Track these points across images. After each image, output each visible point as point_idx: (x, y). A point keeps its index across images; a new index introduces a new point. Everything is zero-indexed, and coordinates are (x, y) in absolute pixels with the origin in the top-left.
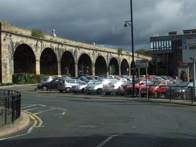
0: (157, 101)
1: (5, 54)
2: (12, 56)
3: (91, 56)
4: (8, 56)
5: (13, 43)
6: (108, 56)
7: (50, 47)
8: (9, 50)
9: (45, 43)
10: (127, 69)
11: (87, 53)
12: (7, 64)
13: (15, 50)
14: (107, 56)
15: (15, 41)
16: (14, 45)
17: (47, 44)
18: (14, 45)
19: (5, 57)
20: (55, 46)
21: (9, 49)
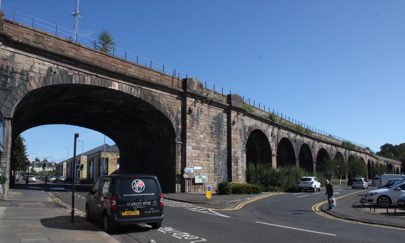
8: (241, 138)
20: (292, 135)
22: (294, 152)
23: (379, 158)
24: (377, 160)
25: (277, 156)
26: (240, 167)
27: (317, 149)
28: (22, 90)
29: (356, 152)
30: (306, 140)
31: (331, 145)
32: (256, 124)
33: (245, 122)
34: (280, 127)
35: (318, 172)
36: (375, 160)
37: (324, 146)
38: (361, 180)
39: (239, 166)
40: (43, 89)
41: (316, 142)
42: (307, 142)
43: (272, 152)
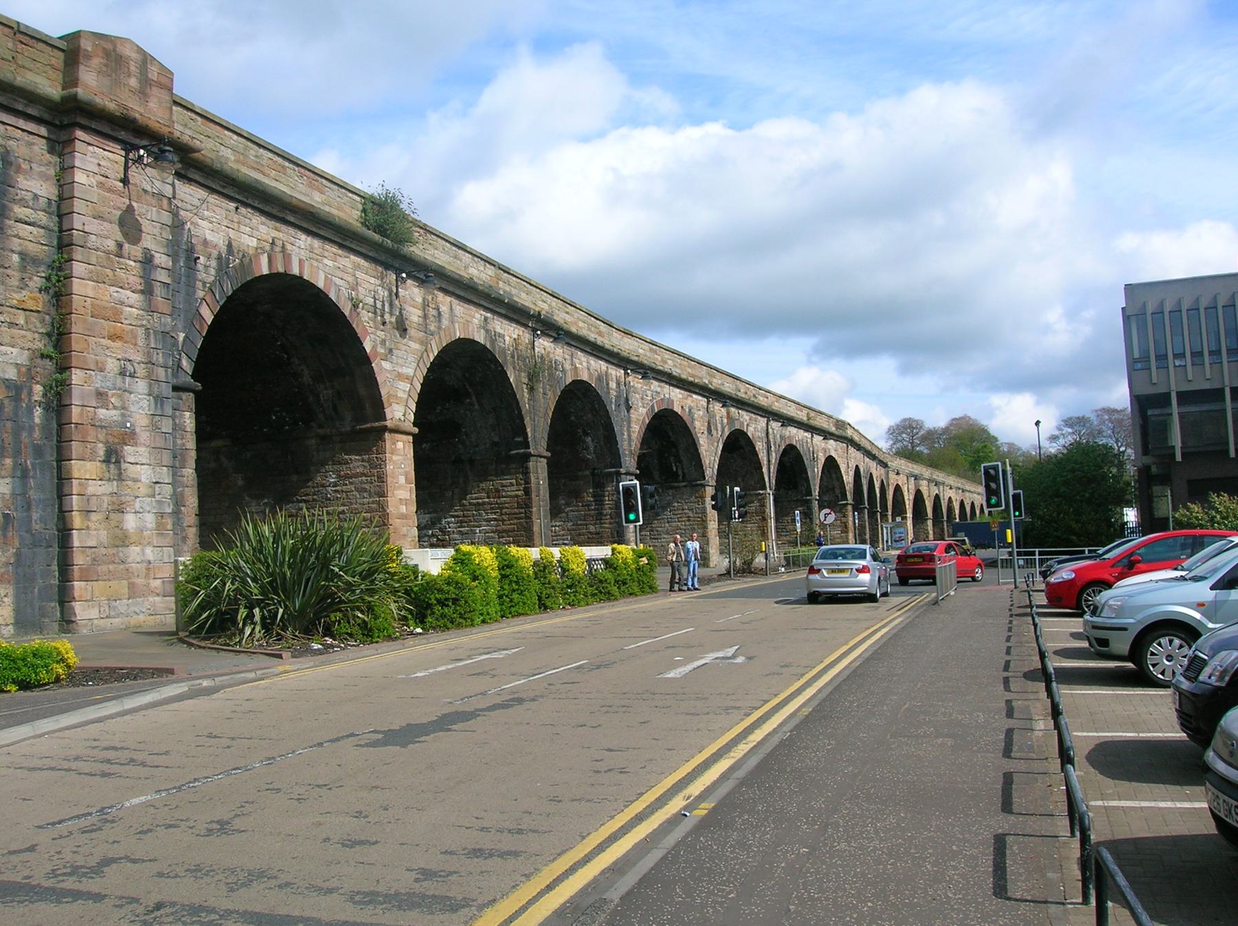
0: (781, 712)
1: (113, 337)
2: (187, 365)
3: (699, 427)
4: (137, 357)
5: (190, 250)
6: (771, 437)
7: (480, 338)
8: (150, 309)
9: (448, 299)
10: (513, 454)
11: (677, 409)
12: (129, 437)
13: (209, 317)
14: (767, 433)
15: (209, 236)
16: (207, 271)
17: (460, 308)
18: (207, 271)
19: (112, 365)
20: (509, 333)
21: (148, 291)
22: (522, 418)
23: (889, 463)
24: (883, 471)
25: (414, 436)
26: (144, 490)
27: (643, 411)
28: (197, 327)
29: (808, 435)
30: (587, 367)
31: (707, 398)
32: (279, 243)
33: (195, 225)
34: (646, 373)
35: (1131, 516)
36: (877, 472)
37: (678, 399)
38: (620, 538)
39: (136, 480)
40: (216, 316)
41: (635, 381)
42: (590, 375)
43: (387, 411)
